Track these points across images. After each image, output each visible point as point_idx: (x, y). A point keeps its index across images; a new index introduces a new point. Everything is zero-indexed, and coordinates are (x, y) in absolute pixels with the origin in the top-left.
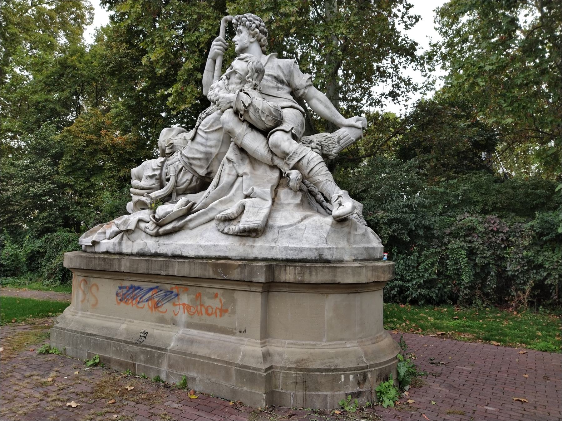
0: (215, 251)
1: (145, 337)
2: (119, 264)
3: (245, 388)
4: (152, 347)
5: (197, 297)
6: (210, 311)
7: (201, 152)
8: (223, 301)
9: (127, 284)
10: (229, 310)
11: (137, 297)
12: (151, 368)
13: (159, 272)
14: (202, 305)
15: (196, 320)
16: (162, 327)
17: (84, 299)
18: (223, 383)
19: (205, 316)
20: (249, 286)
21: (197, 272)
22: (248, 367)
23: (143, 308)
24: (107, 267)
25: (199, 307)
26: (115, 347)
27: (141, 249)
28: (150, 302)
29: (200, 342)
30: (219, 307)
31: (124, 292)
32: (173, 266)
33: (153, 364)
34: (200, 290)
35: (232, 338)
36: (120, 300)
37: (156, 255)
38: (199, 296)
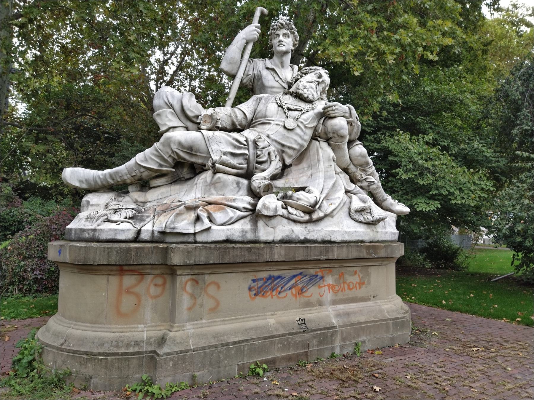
0: (356, 236)
1: (305, 324)
2: (271, 253)
3: (399, 333)
4: (321, 329)
5: (340, 276)
6: (351, 287)
7: (298, 144)
8: (361, 275)
9: (264, 275)
10: (366, 282)
11: (278, 287)
12: (324, 349)
13: (319, 258)
14: (344, 283)
15: (340, 296)
16: (310, 310)
17: (194, 304)
18: (385, 335)
19: (347, 291)
20: (191, 269)
21: (354, 254)
22: (397, 318)
23: (285, 297)
24: (254, 258)
25: (342, 285)
26: (281, 344)
27: (287, 236)
28: (293, 290)
29: (354, 313)
30: (358, 281)
31: (259, 285)
32: (333, 251)
33: (327, 344)
34: (342, 270)
35: (370, 303)
36: (255, 295)
37: (306, 241)
38: (341, 275)
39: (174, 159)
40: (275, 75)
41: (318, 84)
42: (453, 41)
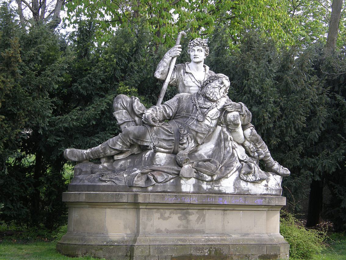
39: (130, 143)
40: (192, 78)
41: (221, 88)
42: (257, 108)
